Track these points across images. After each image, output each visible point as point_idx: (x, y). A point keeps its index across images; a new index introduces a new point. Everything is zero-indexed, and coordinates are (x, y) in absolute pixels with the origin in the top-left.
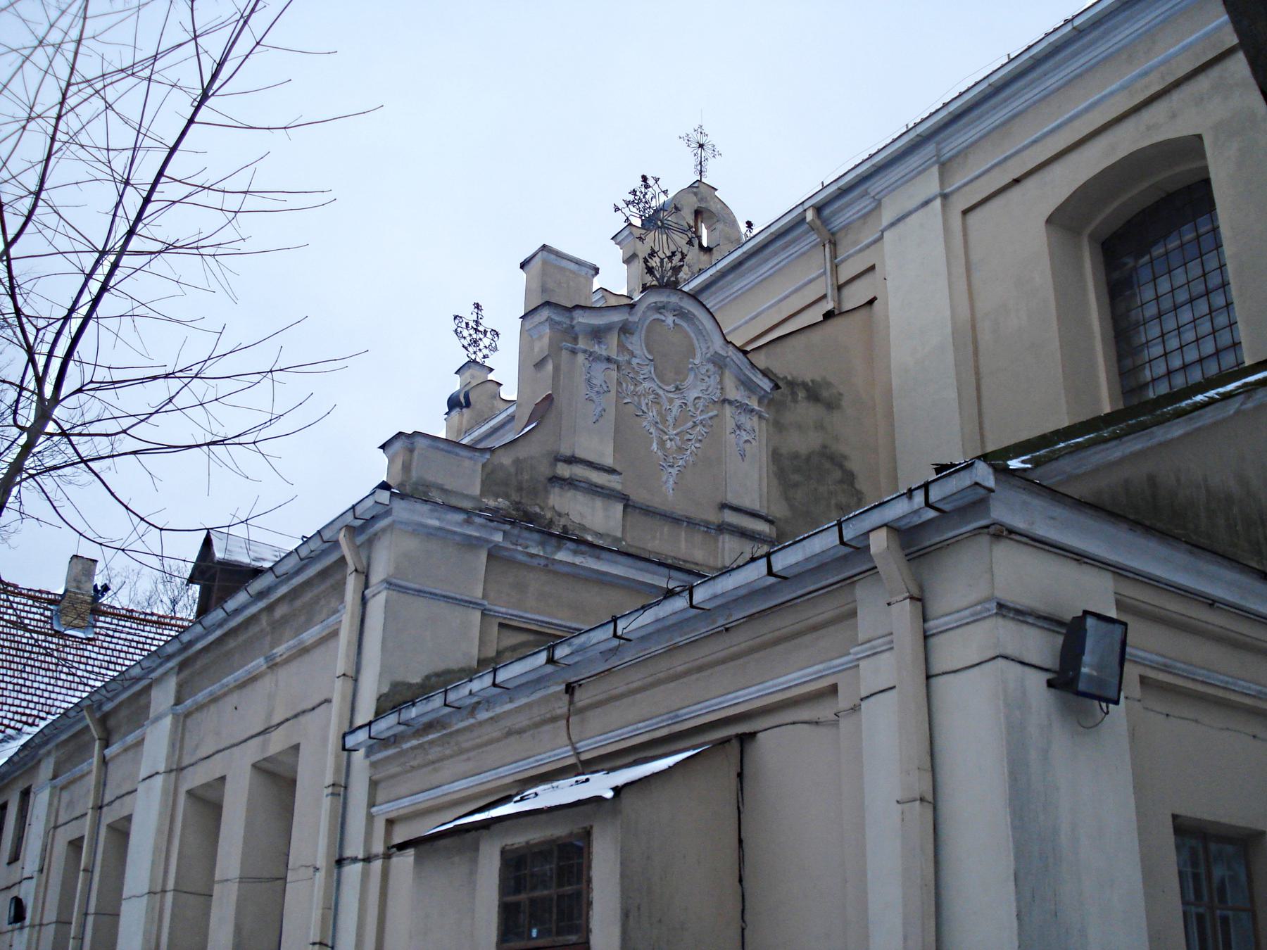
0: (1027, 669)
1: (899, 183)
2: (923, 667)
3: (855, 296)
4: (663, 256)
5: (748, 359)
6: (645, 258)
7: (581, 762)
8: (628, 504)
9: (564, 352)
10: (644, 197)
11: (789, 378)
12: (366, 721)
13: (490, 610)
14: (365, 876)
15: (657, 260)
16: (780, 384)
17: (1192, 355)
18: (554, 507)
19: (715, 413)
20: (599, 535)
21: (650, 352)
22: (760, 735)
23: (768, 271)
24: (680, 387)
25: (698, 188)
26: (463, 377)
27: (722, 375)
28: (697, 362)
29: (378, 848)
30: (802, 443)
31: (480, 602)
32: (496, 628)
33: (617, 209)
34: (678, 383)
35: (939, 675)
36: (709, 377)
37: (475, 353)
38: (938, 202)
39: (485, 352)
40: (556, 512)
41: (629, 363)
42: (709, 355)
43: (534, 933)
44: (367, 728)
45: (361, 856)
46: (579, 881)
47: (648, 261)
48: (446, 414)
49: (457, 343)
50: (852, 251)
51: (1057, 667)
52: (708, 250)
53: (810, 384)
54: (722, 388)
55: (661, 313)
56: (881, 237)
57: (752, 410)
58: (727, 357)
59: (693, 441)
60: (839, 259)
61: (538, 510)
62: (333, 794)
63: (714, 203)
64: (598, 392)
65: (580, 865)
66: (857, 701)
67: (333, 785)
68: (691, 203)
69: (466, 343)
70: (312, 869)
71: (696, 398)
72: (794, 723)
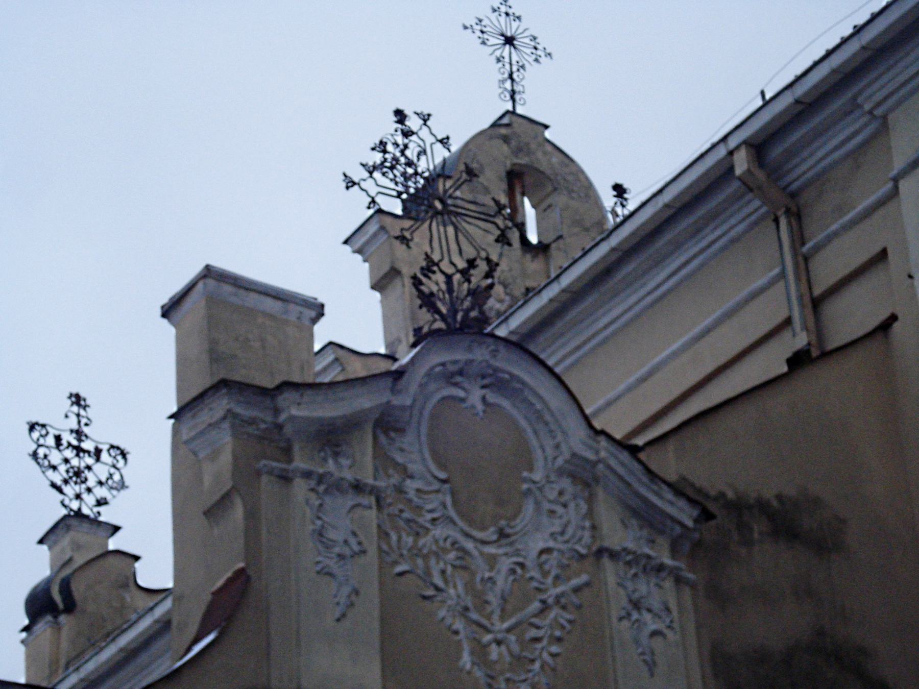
6: (414, 277)
10: (403, 153)
16: (712, 507)
19: (584, 578)
21: (442, 466)
27: (591, 500)
28: (538, 476)
33: (350, 183)
36: (565, 506)
37: (78, 497)
39: (101, 492)
41: (400, 490)
42: (560, 461)
47: (421, 283)
48: (26, 629)
49: (39, 480)
50: (834, 227)
54: (594, 527)
55: (456, 385)
56: (895, 193)
57: (660, 568)
59: (545, 642)
60: (809, 245)
63: (545, 153)
64: (341, 557)
71: (543, 552)
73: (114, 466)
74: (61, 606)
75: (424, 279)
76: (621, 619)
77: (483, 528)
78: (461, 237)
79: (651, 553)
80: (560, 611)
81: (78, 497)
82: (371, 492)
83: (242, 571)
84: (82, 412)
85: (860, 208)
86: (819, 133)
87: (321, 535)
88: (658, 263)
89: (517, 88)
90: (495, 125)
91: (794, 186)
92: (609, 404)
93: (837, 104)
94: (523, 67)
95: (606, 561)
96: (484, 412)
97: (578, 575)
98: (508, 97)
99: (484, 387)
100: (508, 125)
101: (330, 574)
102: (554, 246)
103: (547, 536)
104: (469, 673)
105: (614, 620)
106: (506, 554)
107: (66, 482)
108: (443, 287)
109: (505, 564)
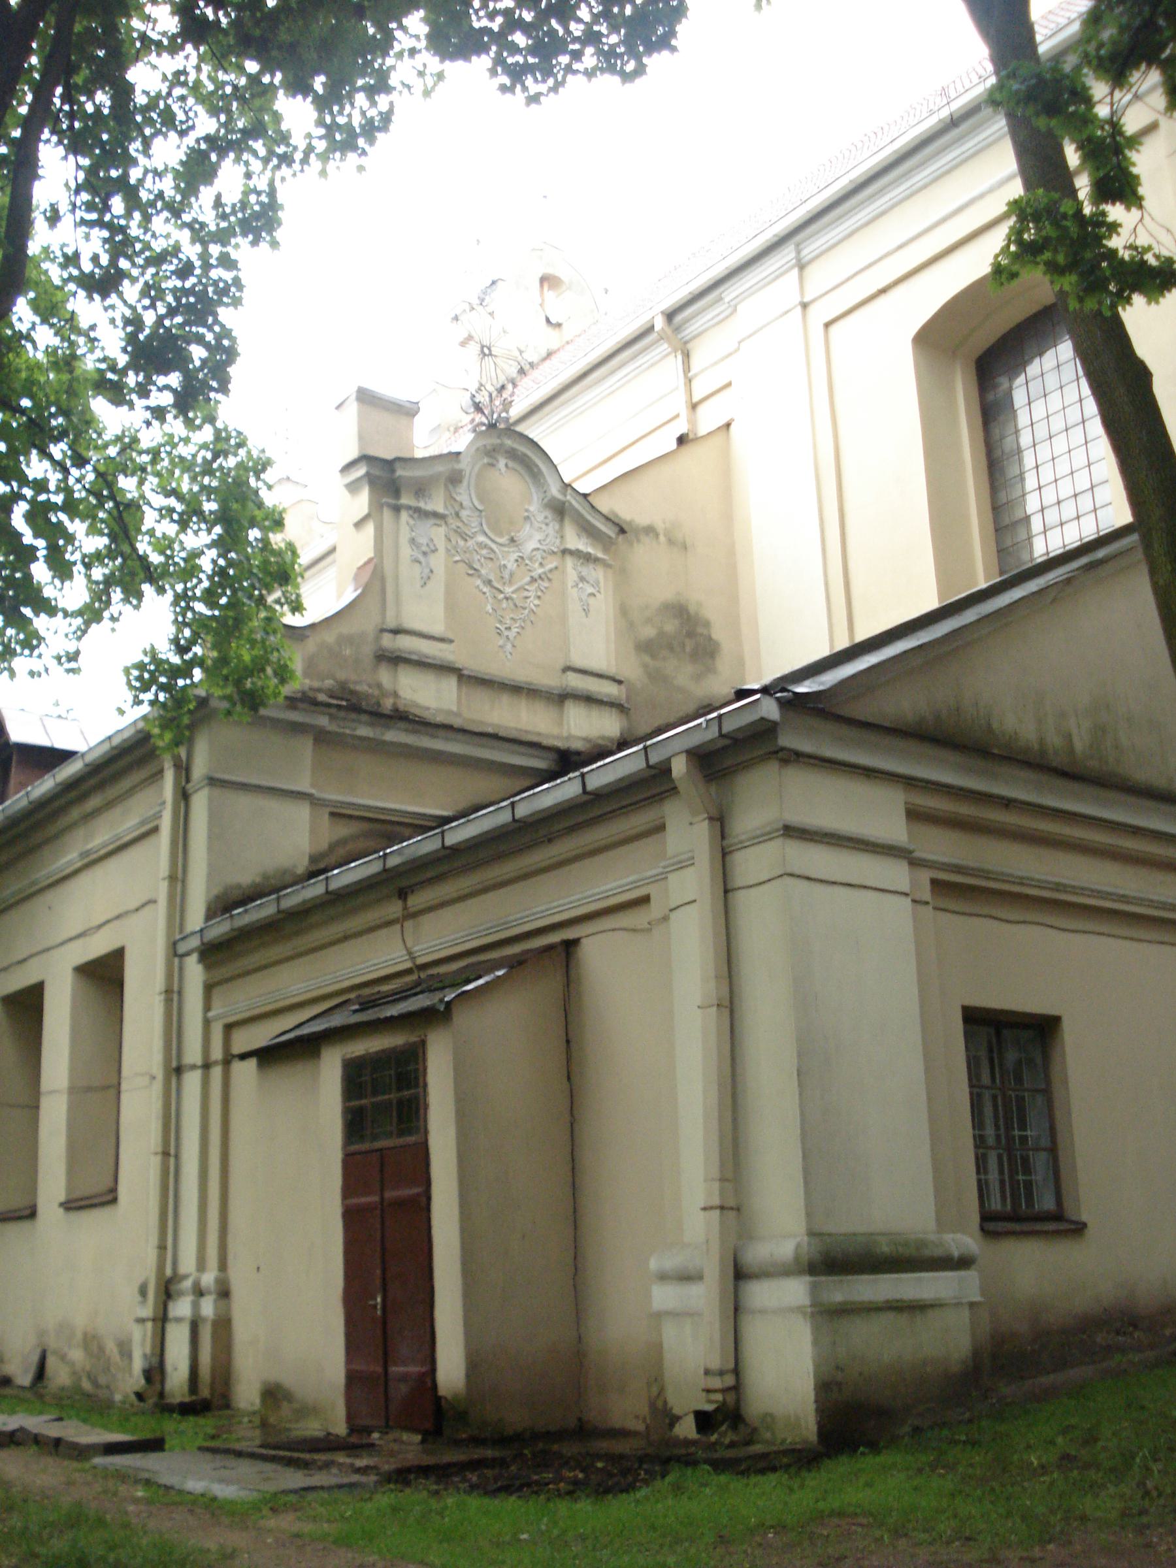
1: (746, 294)
2: (722, 884)
3: (707, 421)
4: (490, 388)
5: (589, 502)
9: (385, 509)
15: (486, 394)
17: (1066, 490)
21: (482, 501)
22: (584, 941)
29: (217, 1053)
32: (327, 816)
35: (743, 888)
36: (547, 525)
41: (457, 514)
46: (417, 1086)
59: (531, 599)
65: (416, 1070)
66: (667, 912)
72: (613, 930)
76: (572, 587)
77: (501, 535)
78: (498, 370)
91: (687, 338)
97: (552, 563)
101: (420, 563)
108: (487, 399)
109: (515, 556)
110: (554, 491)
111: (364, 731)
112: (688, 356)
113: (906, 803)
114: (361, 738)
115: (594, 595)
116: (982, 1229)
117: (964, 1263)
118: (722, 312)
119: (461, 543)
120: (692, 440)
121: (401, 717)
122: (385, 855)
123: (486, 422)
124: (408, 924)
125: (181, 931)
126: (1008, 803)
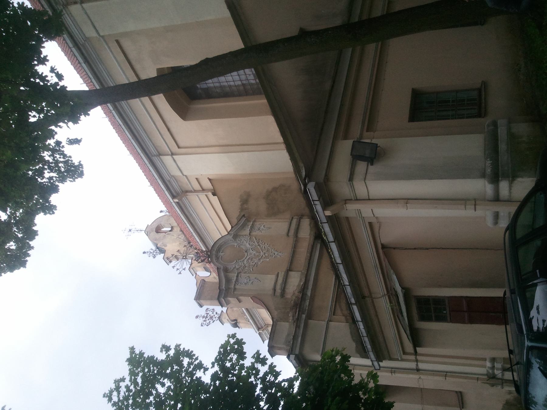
0: (368, 172)
6: (198, 263)
7: (387, 294)
8: (289, 270)
10: (151, 253)
11: (240, 210)
12: (371, 362)
13: (329, 319)
14: (422, 362)
16: (242, 214)
18: (291, 296)
19: (254, 238)
20: (300, 281)
21: (233, 261)
22: (382, 243)
23: (194, 214)
24: (246, 250)
25: (148, 232)
26: (225, 322)
27: (240, 236)
28: (236, 245)
29: (413, 357)
30: (263, 206)
31: (326, 323)
32: (334, 316)
34: (244, 251)
36: (241, 240)
37: (215, 318)
38: (174, 157)
39: (215, 313)
40: (293, 295)
41: (238, 269)
42: (233, 240)
43: (445, 312)
44: (373, 362)
45: (416, 363)
47: (199, 262)
48: (239, 328)
49: (212, 325)
50: (190, 186)
51: (366, 163)
52: (172, 228)
53: (241, 203)
54: (245, 235)
55: (219, 257)
56: (186, 176)
57: (253, 224)
58: (234, 233)
60: (193, 190)
61: (292, 302)
62: (394, 373)
63: (153, 225)
64: (249, 280)
67: (391, 373)
68: (154, 234)
69: (212, 321)
70: (419, 379)
71: (249, 245)
73: (210, 311)
74: (236, 321)
75: (199, 261)
76: (261, 232)
79: (250, 226)
80: (260, 243)
81: (215, 318)
82: (238, 274)
83: (251, 297)
84: (199, 316)
85: (188, 182)
86: (172, 185)
87: (245, 284)
88: (191, 215)
89: (140, 230)
90: (147, 235)
92: (216, 226)
93: (168, 183)
94: (135, 228)
95: (251, 234)
96: (224, 253)
98: (141, 232)
99: (219, 252)
100: (147, 232)
102: (172, 225)
103: (247, 244)
104: (270, 259)
105: (262, 233)
106: (250, 251)
107: (212, 320)
109: (251, 251)
110: (230, 237)
111: (307, 303)
112: (187, 191)
113: (342, 140)
114: (309, 304)
115: (264, 225)
116: (483, 117)
117: (495, 124)
118: (173, 180)
119: (247, 268)
120: (214, 190)
121: (303, 289)
122: (362, 336)
123: (207, 258)
124: (373, 296)
125: (372, 367)
126: (342, 105)
